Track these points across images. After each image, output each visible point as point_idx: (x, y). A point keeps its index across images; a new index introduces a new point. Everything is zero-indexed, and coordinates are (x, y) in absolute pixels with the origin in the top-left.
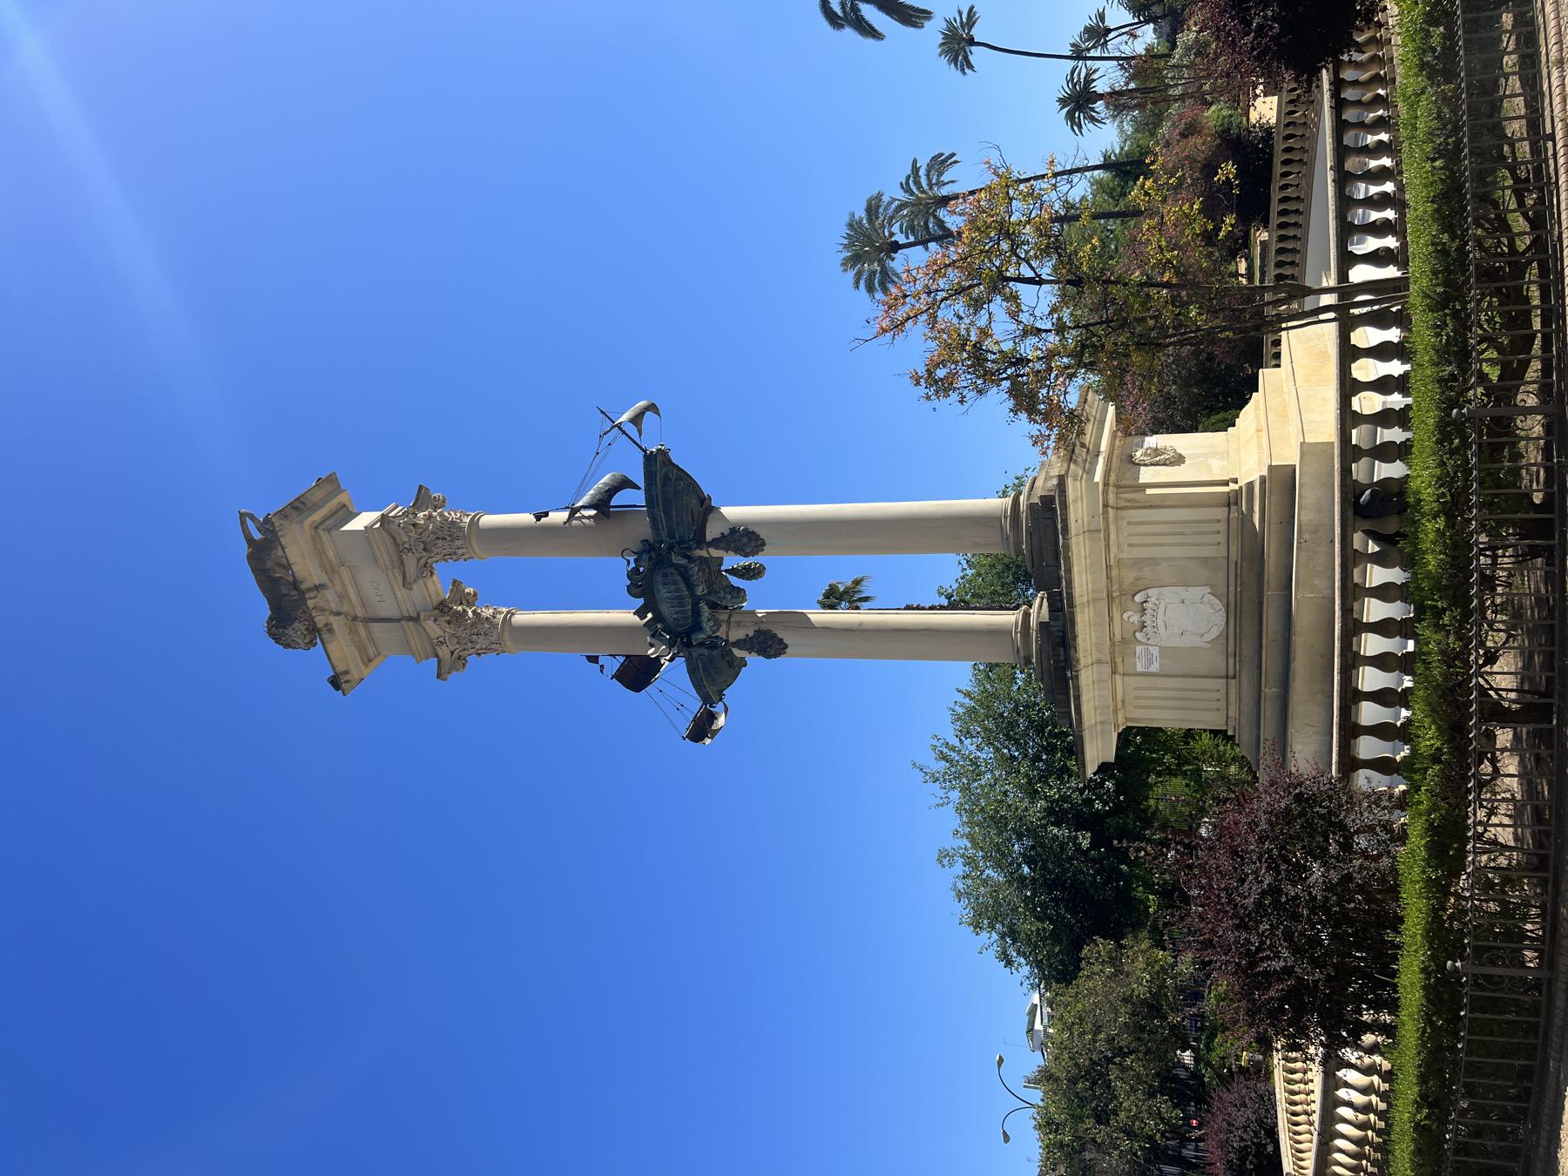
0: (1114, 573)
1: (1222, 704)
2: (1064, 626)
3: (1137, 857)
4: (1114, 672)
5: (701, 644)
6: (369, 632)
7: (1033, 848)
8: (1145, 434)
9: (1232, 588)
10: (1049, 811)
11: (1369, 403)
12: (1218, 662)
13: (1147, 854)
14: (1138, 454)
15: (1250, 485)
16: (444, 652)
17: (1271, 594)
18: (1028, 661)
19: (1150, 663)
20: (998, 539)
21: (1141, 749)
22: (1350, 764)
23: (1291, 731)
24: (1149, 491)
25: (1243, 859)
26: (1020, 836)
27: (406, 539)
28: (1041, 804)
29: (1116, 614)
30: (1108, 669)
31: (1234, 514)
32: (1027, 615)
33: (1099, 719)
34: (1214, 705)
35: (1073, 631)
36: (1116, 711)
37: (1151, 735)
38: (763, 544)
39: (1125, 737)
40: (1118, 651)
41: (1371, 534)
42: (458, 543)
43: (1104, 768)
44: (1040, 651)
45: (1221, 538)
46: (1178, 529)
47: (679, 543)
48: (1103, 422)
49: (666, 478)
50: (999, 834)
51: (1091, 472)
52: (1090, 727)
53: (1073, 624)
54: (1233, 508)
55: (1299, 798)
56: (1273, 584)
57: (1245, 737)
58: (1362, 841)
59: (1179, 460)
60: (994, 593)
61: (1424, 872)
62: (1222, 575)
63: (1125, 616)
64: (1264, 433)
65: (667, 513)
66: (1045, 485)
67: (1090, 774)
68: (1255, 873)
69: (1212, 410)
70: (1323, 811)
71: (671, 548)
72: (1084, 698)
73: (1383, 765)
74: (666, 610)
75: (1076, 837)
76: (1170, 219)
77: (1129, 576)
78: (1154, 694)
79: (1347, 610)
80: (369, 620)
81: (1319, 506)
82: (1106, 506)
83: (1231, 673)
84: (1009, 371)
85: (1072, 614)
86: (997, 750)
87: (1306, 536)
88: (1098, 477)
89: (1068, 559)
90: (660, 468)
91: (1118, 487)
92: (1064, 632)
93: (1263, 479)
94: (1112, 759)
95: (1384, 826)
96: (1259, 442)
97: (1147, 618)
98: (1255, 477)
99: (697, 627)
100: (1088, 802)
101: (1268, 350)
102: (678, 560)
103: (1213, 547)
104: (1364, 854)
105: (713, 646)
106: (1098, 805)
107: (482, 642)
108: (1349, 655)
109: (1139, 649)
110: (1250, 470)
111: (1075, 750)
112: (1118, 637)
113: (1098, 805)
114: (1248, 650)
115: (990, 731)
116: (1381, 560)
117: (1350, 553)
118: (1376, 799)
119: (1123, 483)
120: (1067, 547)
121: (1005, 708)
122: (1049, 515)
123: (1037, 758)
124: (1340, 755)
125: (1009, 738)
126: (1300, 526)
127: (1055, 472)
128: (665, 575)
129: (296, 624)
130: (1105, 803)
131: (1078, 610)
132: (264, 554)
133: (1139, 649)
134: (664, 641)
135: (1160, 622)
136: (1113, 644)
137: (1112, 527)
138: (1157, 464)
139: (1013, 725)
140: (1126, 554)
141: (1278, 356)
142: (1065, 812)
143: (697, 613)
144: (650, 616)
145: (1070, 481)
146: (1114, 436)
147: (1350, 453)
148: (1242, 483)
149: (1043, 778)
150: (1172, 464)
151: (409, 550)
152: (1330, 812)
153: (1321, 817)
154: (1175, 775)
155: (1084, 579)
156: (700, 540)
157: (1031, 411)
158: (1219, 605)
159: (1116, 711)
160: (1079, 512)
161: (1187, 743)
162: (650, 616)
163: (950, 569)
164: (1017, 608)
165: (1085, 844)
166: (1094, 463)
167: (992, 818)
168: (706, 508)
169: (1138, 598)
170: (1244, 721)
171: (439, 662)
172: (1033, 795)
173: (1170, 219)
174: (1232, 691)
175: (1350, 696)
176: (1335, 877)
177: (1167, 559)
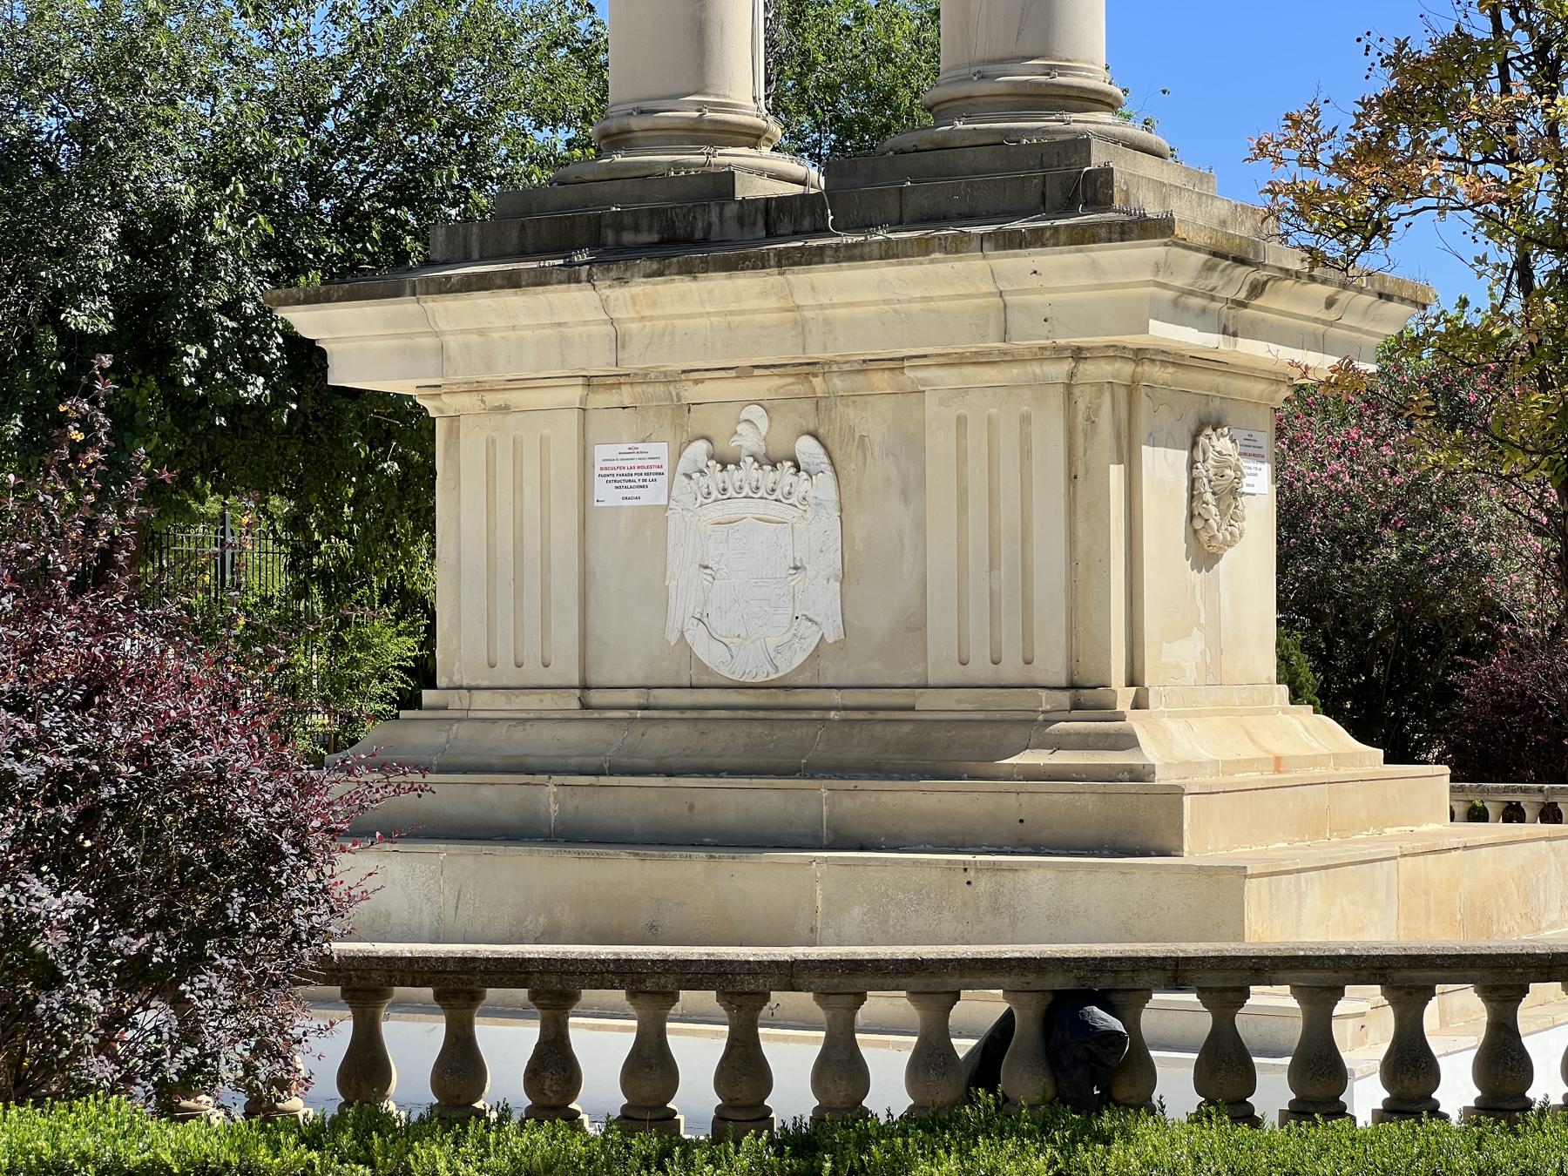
0: (882, 381)
1: (510, 677)
2: (724, 242)
3: (61, 421)
4: (589, 382)
7: (51, 169)
8: (1279, 468)
10: (166, 219)
11: (1363, 1027)
12: (627, 661)
13: (78, 449)
14: (1224, 444)
15: (1128, 741)
17: (822, 799)
18: (617, 140)
19: (622, 480)
20: (981, 52)
21: (363, 472)
22: (365, 987)
23: (443, 852)
24: (1116, 473)
25: (78, 707)
26: (82, 132)
28: (186, 198)
29: (761, 386)
30: (600, 365)
31: (1046, 701)
32: (753, 137)
33: (452, 342)
34: (504, 655)
35: (707, 267)
36: (477, 388)
37: (412, 499)
39: (402, 427)
40: (656, 395)
41: (998, 1039)
43: (307, 357)
44: (646, 176)
45: (980, 669)
46: (1009, 550)
50: (88, 72)
51: (1178, 311)
52: (427, 318)
53: (729, 266)
54: (1064, 698)
55: (267, 851)
57: (415, 733)
58: (153, 1016)
59: (1204, 554)
60: (808, 65)
61: (84, 1159)
62: (876, 671)
63: (755, 412)
64: (1269, 777)
66: (1140, 184)
67: (284, 313)
68: (44, 740)
69: (1323, 662)
70: (233, 912)
72: (509, 300)
73: (365, 1068)
75: (95, 293)
77: (872, 421)
78: (531, 492)
79: (791, 975)
81: (1073, 912)
82: (1078, 354)
83: (595, 697)
84: (1521, 36)
85: (760, 263)
86: (337, 67)
87: (984, 884)
88: (1163, 332)
89: (923, 249)
91: (1132, 388)
92: (706, 242)
93: (1139, 774)
94: (339, 376)
95: (196, 1067)
96: (1249, 764)
97: (749, 472)
98: (1150, 752)
100: (202, 330)
101: (1495, 794)
103: (960, 648)
104: (117, 1020)
106: (194, 354)
108: (669, 982)
109: (659, 451)
110: (1173, 739)
111: (349, 279)
112: (691, 393)
113: (194, 354)
114: (659, 740)
115: (394, 45)
116: (931, 1059)
117: (951, 982)
118: (271, 1047)
119: (1131, 399)
120: (955, 247)
121: (464, 89)
122: (1055, 194)
123: (319, 184)
124: (389, 962)
125: (377, 101)
126: (1012, 869)
127: (1182, 211)
130: (202, 376)
131: (769, 280)
133: (659, 451)
135: (735, 508)
136: (669, 379)
137: (1016, 371)
139: (415, 113)
140: (937, 418)
141: (1477, 815)
142: (167, 262)
147: (1225, 980)
148: (1135, 722)
149: (263, 199)
152: (230, 930)
153: (218, 910)
154: (292, 567)
155: (861, 296)
157: (1397, 107)
158: (789, 664)
159: (477, 388)
160: (1060, 281)
161: (386, 598)
165: (77, 319)
166: (1201, 319)
167: (133, 48)
169: (807, 448)
170: (461, 731)
172: (213, 174)
174: (548, 701)
175: (554, 982)
176: (51, 943)
177: (920, 527)
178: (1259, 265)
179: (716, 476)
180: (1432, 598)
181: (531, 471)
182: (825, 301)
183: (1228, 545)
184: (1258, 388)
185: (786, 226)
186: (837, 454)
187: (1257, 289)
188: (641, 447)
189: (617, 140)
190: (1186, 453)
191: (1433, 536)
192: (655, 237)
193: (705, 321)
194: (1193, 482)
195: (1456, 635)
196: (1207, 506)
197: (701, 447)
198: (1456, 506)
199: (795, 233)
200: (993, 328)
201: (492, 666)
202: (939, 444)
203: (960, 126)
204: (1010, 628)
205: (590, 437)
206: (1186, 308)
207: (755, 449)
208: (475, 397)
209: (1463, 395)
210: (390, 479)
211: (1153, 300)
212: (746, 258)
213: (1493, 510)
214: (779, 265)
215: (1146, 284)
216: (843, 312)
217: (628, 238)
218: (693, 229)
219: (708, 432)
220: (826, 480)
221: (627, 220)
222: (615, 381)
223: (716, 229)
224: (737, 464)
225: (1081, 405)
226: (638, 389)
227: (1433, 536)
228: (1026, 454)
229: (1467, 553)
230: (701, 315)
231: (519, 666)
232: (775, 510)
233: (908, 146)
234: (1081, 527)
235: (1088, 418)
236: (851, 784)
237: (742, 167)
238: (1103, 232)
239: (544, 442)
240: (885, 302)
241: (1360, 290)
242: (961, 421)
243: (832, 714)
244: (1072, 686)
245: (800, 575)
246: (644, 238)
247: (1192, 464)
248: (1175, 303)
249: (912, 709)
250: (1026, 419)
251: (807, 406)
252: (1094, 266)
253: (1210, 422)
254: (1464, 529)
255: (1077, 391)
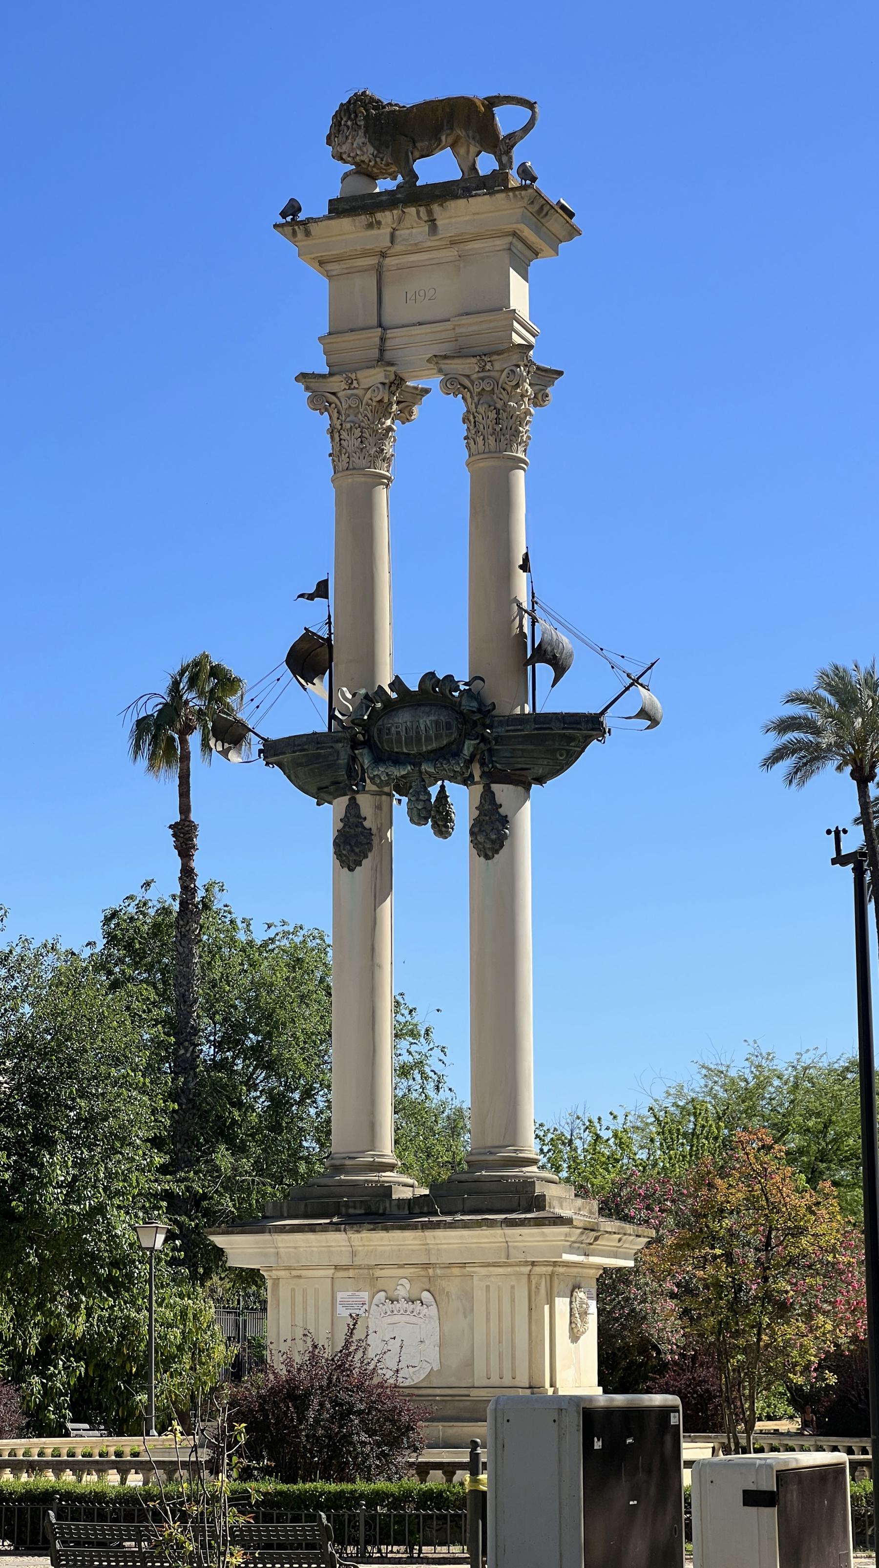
0: (456, 1271)
4: (337, 1268)
5: (354, 758)
6: (363, 270)
9: (438, 1392)
14: (582, 1295)
16: (337, 384)
18: (338, 1169)
24: (547, 1307)
27: (498, 366)
30: (346, 1261)
32: (391, 1167)
33: (282, 1250)
35: (393, 1228)
36: (288, 1268)
38: (487, 857)
40: (367, 1275)
42: (491, 440)
44: (355, 1185)
45: (495, 1380)
47: (490, 750)
48: (616, 1256)
49: (571, 739)
51: (571, 1250)
53: (402, 1228)
56: (450, 1431)
59: (575, 1337)
62: (452, 1381)
65: (528, 739)
71: (484, 739)
72: (310, 1236)
74: (403, 719)
76: (805, 1341)
77: (452, 1286)
78: (311, 1310)
80: (379, 272)
82: (533, 1264)
85: (414, 1227)
88: (566, 1257)
90: (584, 729)
91: (552, 1275)
99: (379, 759)
102: (468, 747)
105: (351, 773)
107: (351, 442)
109: (365, 1295)
112: (378, 1273)
119: (554, 1280)
122: (524, 1203)
128: (448, 726)
129: (371, 149)
131: (418, 1233)
132: (465, 120)
133: (365, 1295)
134: (359, 709)
135: (396, 1318)
136: (370, 1268)
137: (510, 1269)
138: (571, 1315)
143: (397, 760)
144: (394, 695)
145: (565, 1229)
146: (597, 1267)
150: (571, 1329)
151: (483, 369)
155: (450, 1241)
156: (492, 776)
159: (288, 1268)
160: (529, 1239)
162: (394, 695)
163: (456, 1087)
164: (400, 1157)
168: (524, 781)
169: (426, 1295)
171: (323, 376)
173: (805, 1341)
175: (450, 1469)
178: (598, 1231)
179: (389, 1305)
180: (614, 1337)
181: (311, 1302)
182: (439, 1242)
183: (583, 1333)
184: (593, 1271)
185: (417, 1210)
186: (437, 1299)
187: (596, 1239)
188: (357, 1293)
189: (338, 1169)
190: (568, 1299)
191: (614, 1299)
192: (362, 1212)
193: (389, 1247)
194: (571, 1309)
195: (626, 1358)
196: (576, 1316)
197: (383, 1294)
198: (627, 1283)
199: (421, 1213)
200: (503, 1254)
201: (501, 1378)
202: (479, 1296)
203: (483, 1173)
204: (507, 1365)
205: (335, 1289)
206: (574, 1248)
207: (405, 1295)
208: (287, 1272)
209: (626, 1211)
210: (34, 1268)
211: (564, 1246)
212: (409, 1225)
213: (647, 1284)
214: (422, 1229)
215: (562, 1240)
216: (445, 1246)
217: (351, 1211)
218: (379, 1208)
219: (381, 1288)
220: (433, 1309)
221: (351, 1204)
222: (346, 1268)
223: (388, 1209)
224: (398, 1301)
225: (534, 1282)
226: (357, 1271)
227: (614, 1299)
228: (513, 1300)
229: (633, 1310)
230: (388, 1245)
231: (501, 1378)
232: (413, 1319)
233: (463, 1179)
234: (534, 1328)
235: (536, 1287)
236: (452, 1424)
237: (395, 1183)
238: (547, 1222)
239: (316, 1291)
240: (462, 1243)
241: (630, 1235)
242: (488, 1287)
243: (437, 1398)
244: (530, 1387)
245: (423, 1345)
246: (358, 1211)
247: (571, 1302)
248: (570, 1246)
249: (469, 1396)
250: (513, 1287)
251: (426, 1280)
252: (543, 1234)
253: (576, 1287)
254: (632, 1296)
255: (532, 1277)
